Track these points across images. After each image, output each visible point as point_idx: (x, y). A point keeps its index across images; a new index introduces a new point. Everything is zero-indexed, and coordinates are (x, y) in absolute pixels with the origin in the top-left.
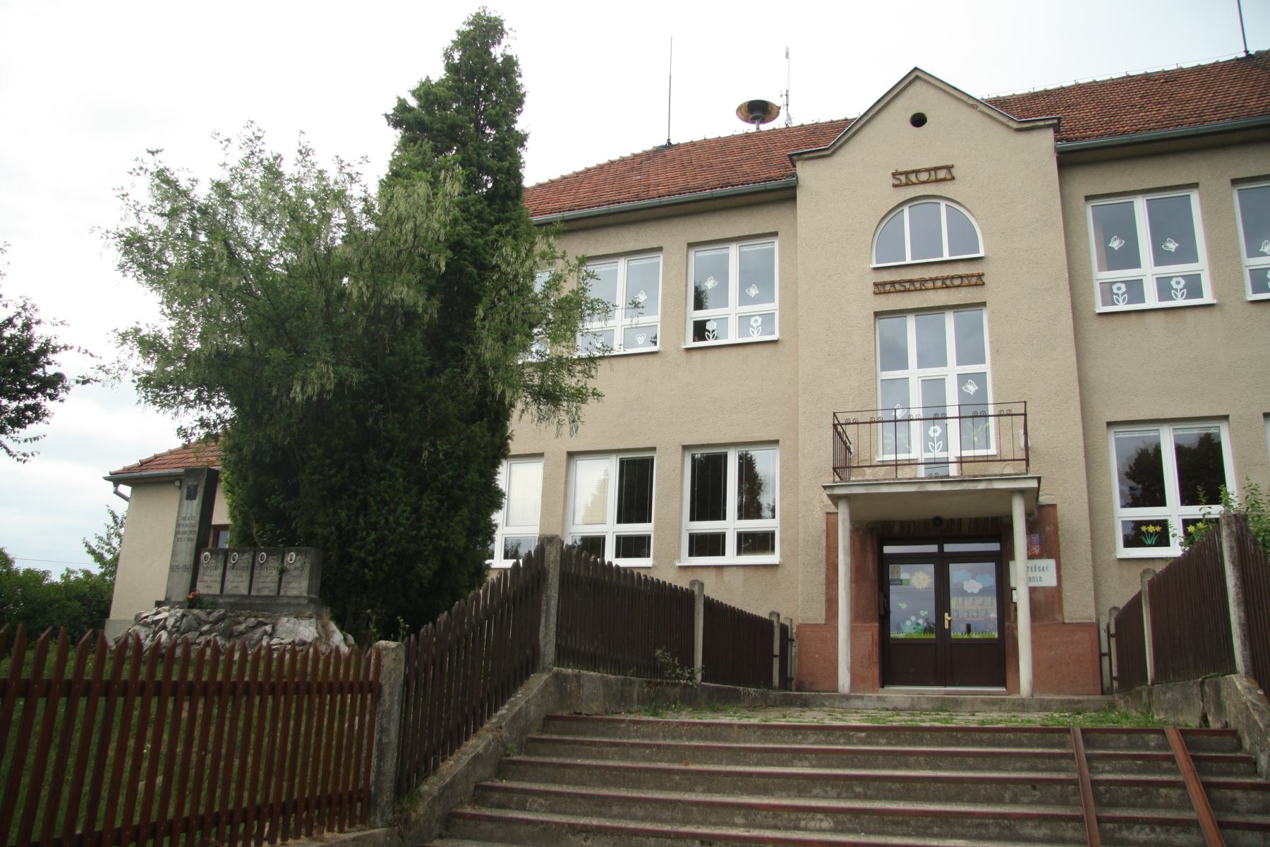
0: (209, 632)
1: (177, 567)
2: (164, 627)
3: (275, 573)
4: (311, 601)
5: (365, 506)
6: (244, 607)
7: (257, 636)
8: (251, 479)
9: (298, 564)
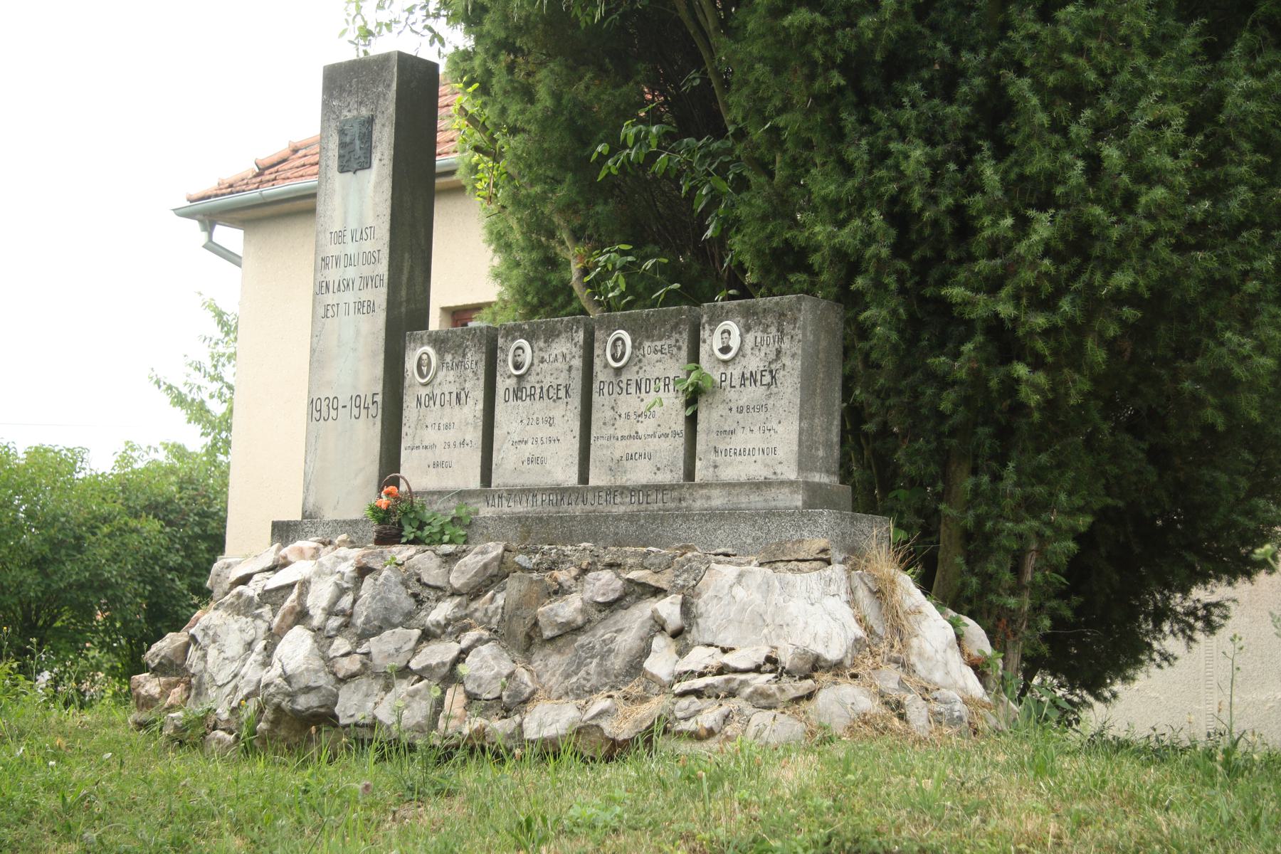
0: (454, 627)
1: (333, 403)
2: (301, 616)
3: (672, 407)
4: (816, 497)
5: (996, 112)
6: (566, 530)
7: (627, 641)
8: (542, 93)
9: (754, 363)
